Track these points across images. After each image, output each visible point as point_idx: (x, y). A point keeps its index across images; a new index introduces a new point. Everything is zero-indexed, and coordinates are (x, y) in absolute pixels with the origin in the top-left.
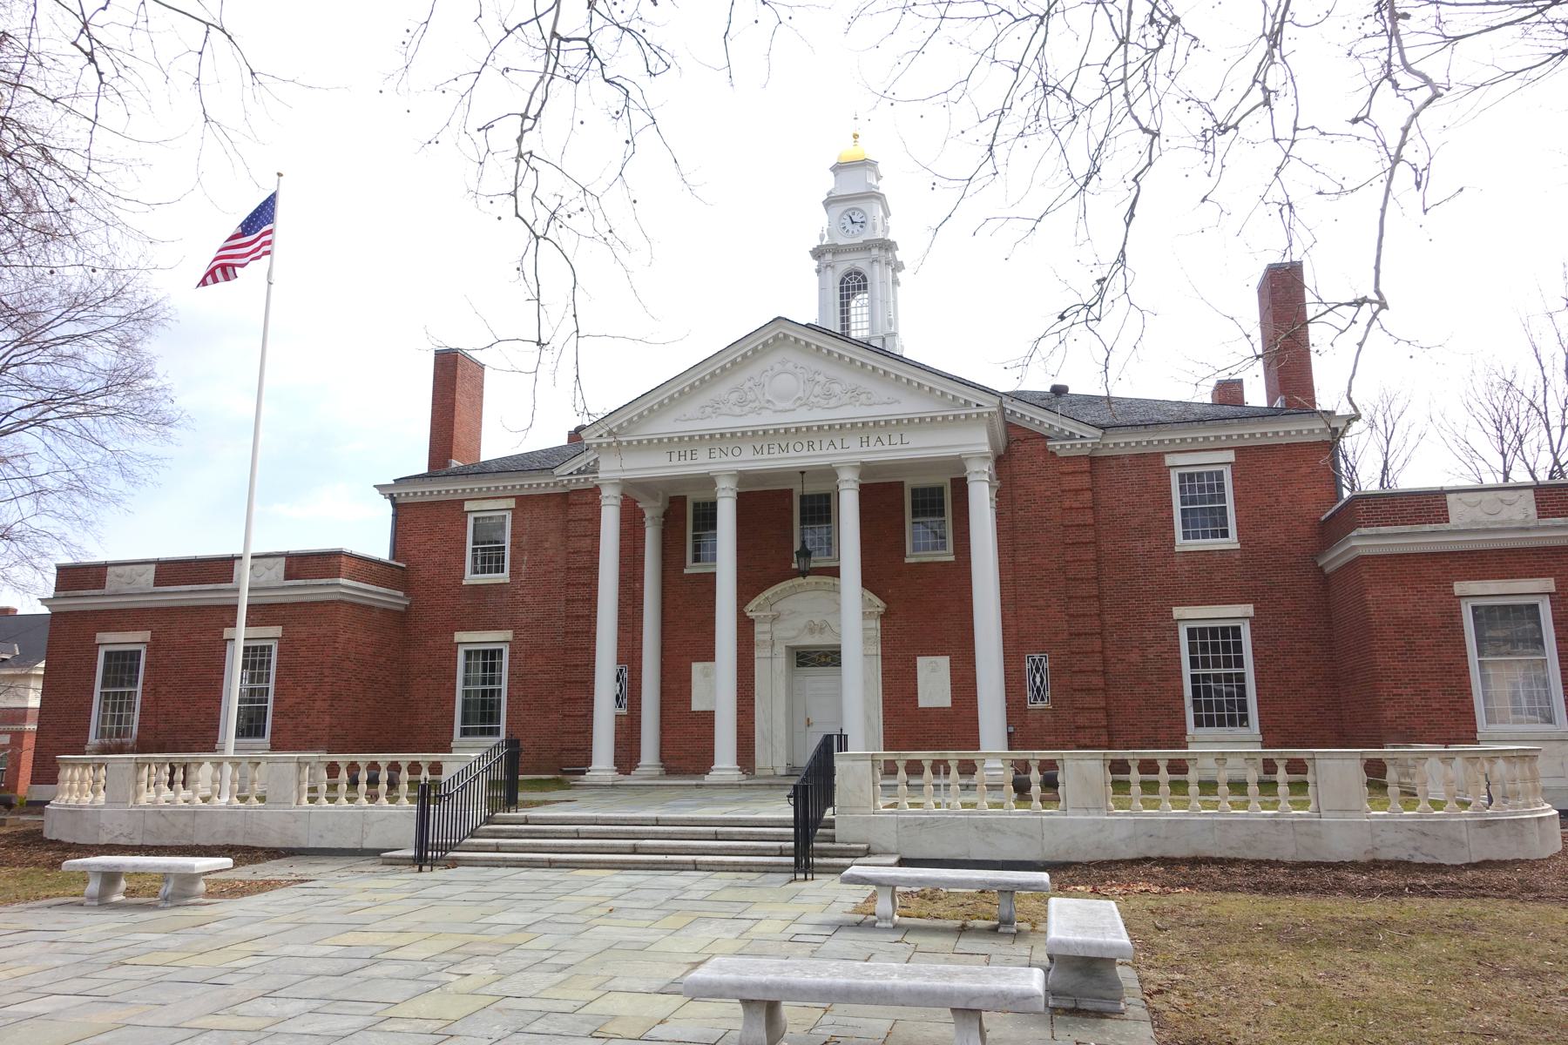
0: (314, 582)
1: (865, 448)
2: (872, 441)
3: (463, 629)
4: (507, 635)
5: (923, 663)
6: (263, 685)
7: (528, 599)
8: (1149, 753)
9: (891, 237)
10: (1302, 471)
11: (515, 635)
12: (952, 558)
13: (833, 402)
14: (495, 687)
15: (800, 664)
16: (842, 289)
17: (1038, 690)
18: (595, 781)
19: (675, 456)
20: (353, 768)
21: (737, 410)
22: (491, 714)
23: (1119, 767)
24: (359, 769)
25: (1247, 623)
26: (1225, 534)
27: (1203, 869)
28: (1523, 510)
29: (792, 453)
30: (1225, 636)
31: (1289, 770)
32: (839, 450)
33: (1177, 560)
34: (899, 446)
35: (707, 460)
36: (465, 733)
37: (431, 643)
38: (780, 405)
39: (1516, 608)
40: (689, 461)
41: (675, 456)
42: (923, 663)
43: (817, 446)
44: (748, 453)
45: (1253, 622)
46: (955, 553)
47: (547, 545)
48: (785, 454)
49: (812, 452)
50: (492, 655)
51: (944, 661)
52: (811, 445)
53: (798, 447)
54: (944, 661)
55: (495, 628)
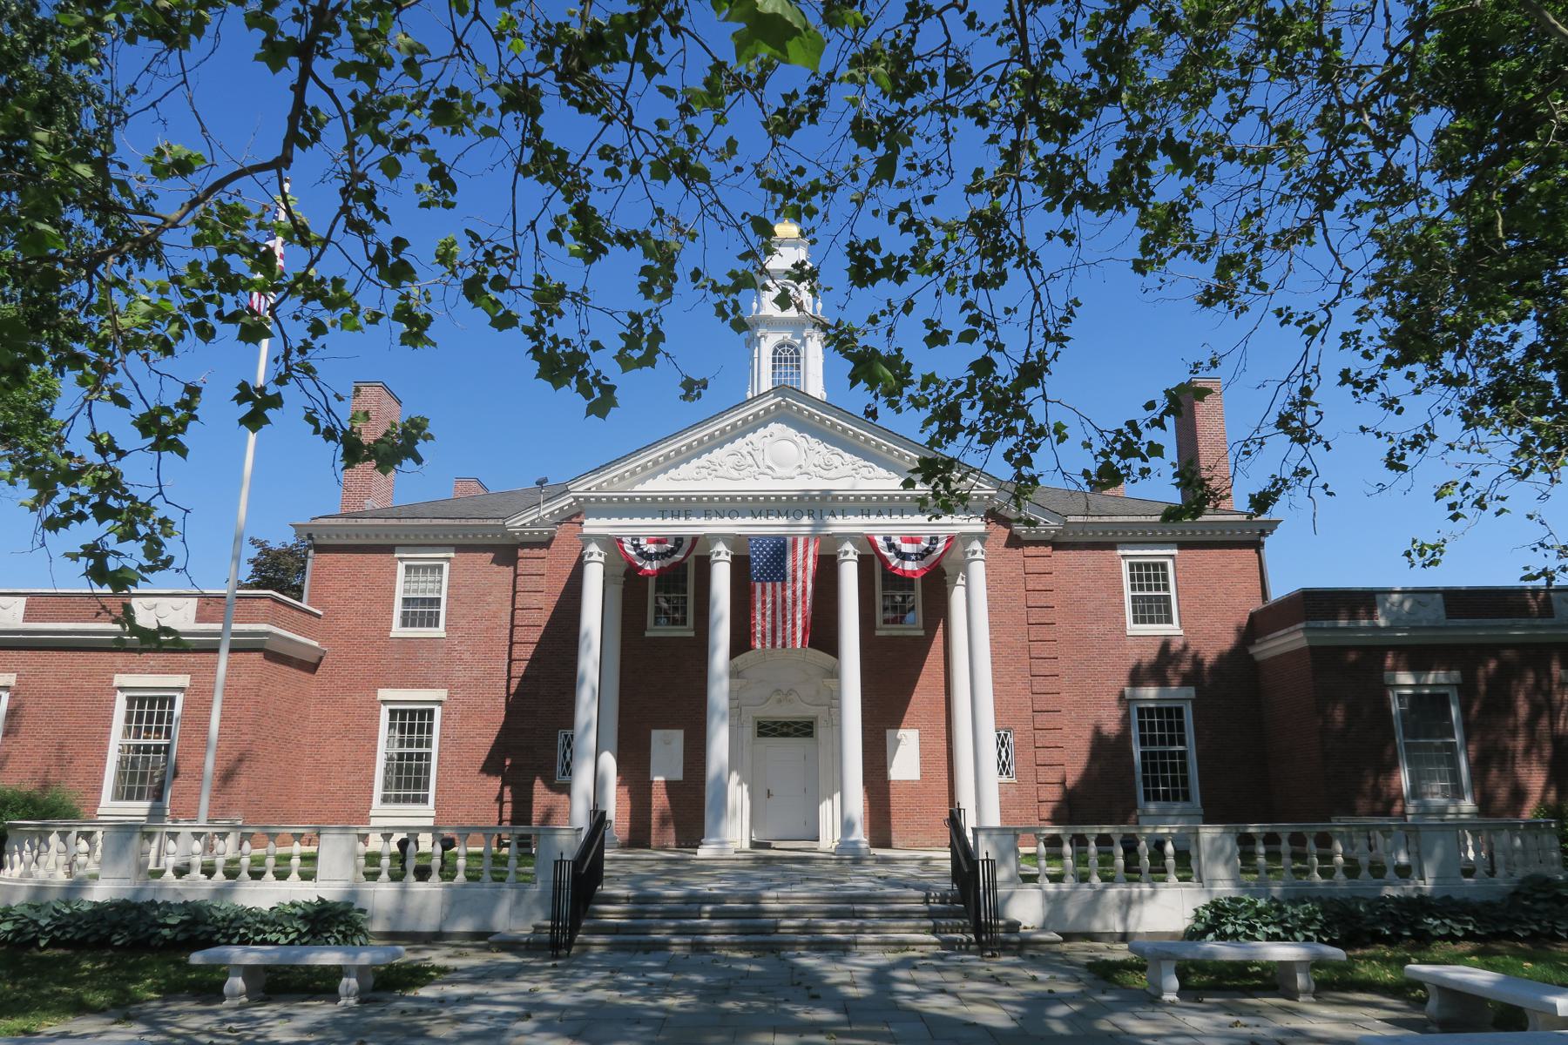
3: (388, 686)
5: (657, 735)
7: (467, 656)
8: (1106, 829)
10: (1236, 566)
12: (692, 634)
13: (832, 474)
14: (424, 750)
15: (761, 734)
16: (774, 360)
21: (735, 474)
22: (418, 781)
23: (1245, 841)
25: (1190, 704)
26: (1169, 620)
28: (1435, 611)
30: (1170, 715)
31: (1318, 845)
33: (1129, 642)
36: (385, 799)
37: (349, 699)
38: (779, 471)
42: (657, 735)
45: (1195, 703)
47: (490, 599)
51: (678, 736)
54: (678, 736)
55: (426, 686)
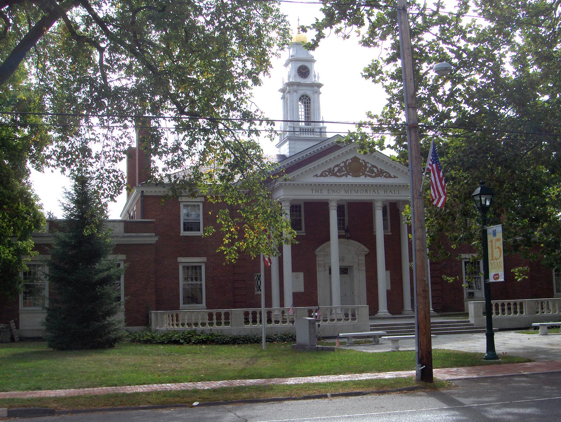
0: (141, 234)
1: (386, 194)
2: (388, 192)
4: (204, 259)
6: (199, 282)
9: (320, 81)
11: (208, 259)
17: (259, 279)
18: (381, 316)
19: (314, 191)
20: (503, 305)
24: (249, 314)
27: (71, 409)
29: (360, 194)
32: (377, 194)
34: (398, 194)
35: (327, 194)
39: (194, 205)
40: (320, 194)
41: (314, 191)
43: (369, 192)
44: (343, 193)
46: (392, 231)
48: (347, 194)
49: (367, 194)
50: (197, 268)
52: (366, 191)
53: (362, 192)
